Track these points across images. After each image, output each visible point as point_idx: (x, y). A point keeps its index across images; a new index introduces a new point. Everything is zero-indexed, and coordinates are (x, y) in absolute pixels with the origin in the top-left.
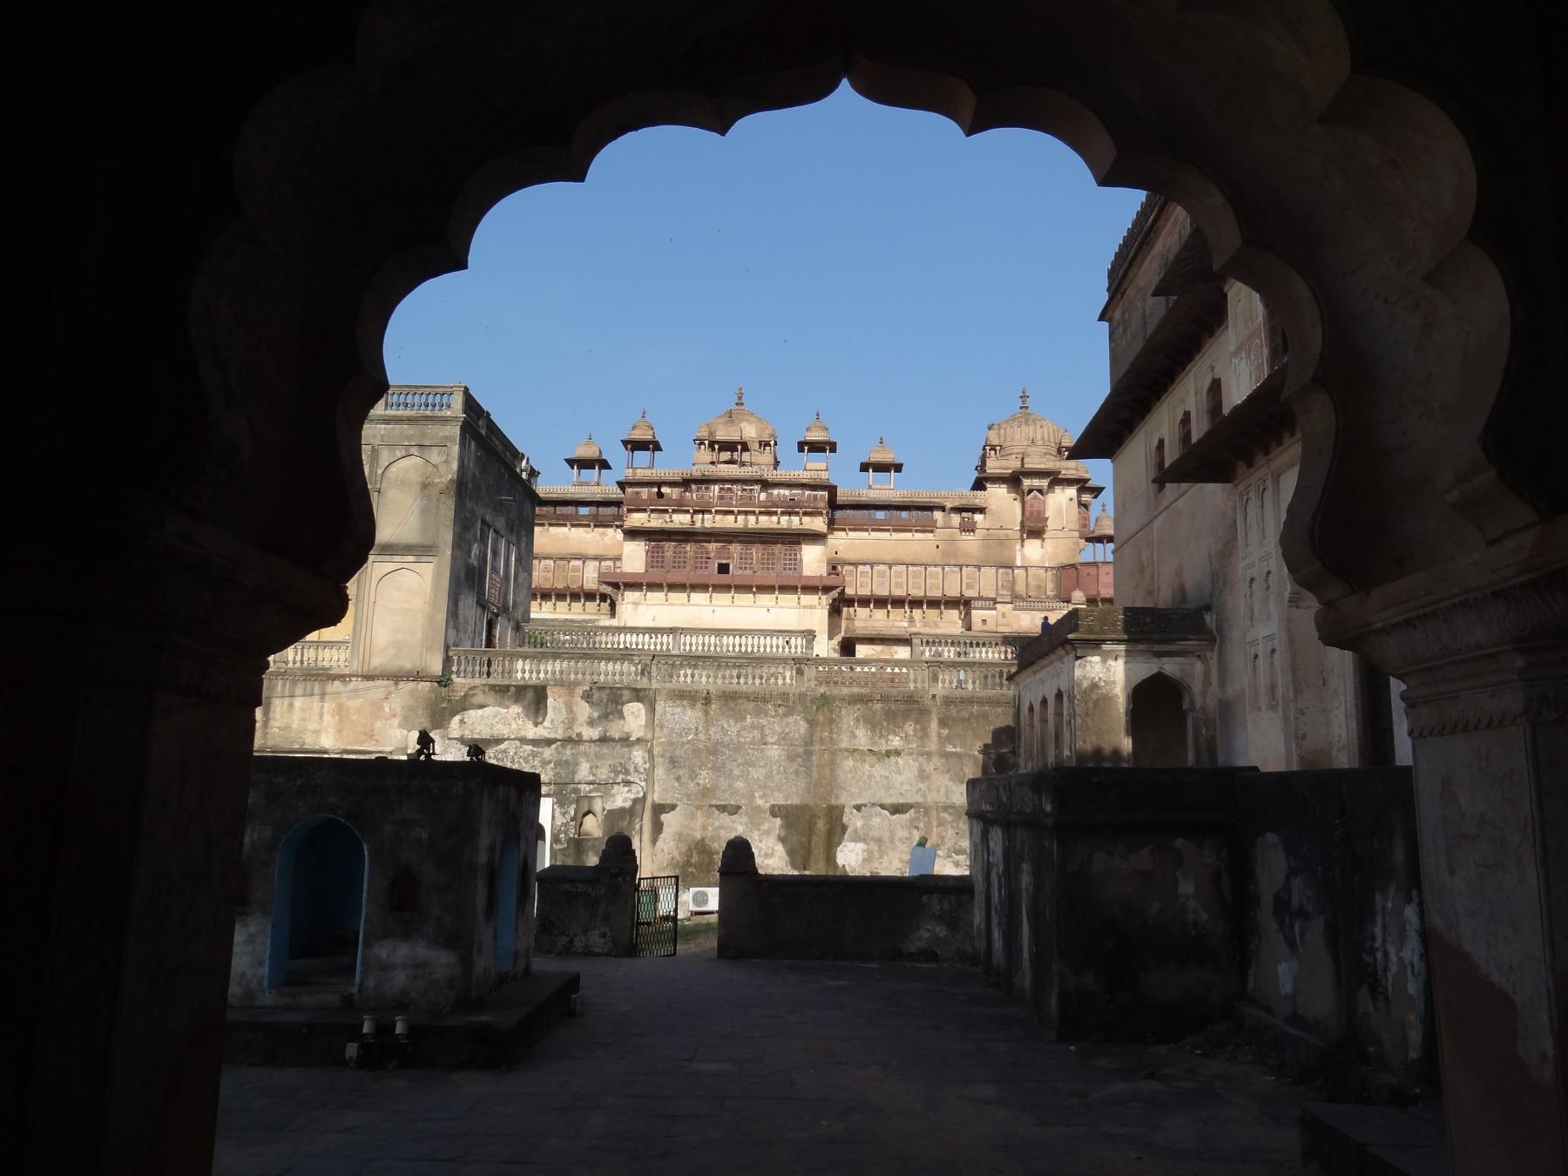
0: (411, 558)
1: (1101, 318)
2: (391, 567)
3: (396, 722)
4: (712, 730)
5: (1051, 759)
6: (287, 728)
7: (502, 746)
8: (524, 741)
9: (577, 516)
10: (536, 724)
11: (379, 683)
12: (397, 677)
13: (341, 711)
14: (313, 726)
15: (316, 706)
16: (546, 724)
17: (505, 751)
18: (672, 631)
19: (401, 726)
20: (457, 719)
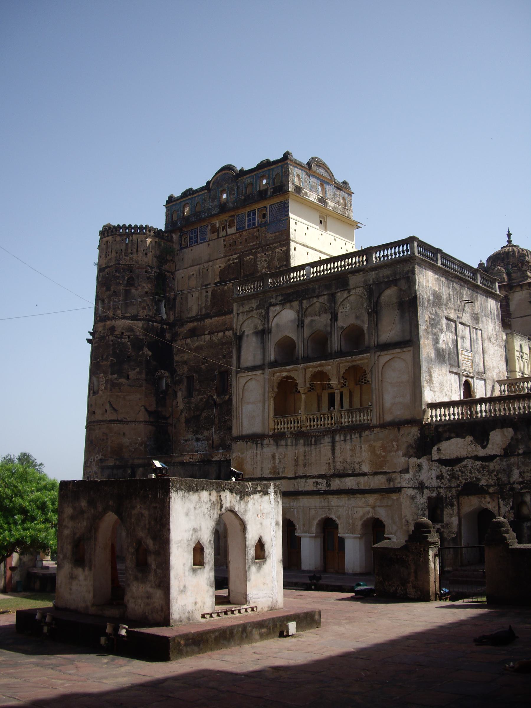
0: (398, 350)
2: (388, 357)
5: (241, 434)
7: (464, 463)
8: (476, 458)
9: (485, 306)
10: (484, 447)
16: (489, 446)
17: (465, 466)
19: (404, 455)
20: (435, 448)
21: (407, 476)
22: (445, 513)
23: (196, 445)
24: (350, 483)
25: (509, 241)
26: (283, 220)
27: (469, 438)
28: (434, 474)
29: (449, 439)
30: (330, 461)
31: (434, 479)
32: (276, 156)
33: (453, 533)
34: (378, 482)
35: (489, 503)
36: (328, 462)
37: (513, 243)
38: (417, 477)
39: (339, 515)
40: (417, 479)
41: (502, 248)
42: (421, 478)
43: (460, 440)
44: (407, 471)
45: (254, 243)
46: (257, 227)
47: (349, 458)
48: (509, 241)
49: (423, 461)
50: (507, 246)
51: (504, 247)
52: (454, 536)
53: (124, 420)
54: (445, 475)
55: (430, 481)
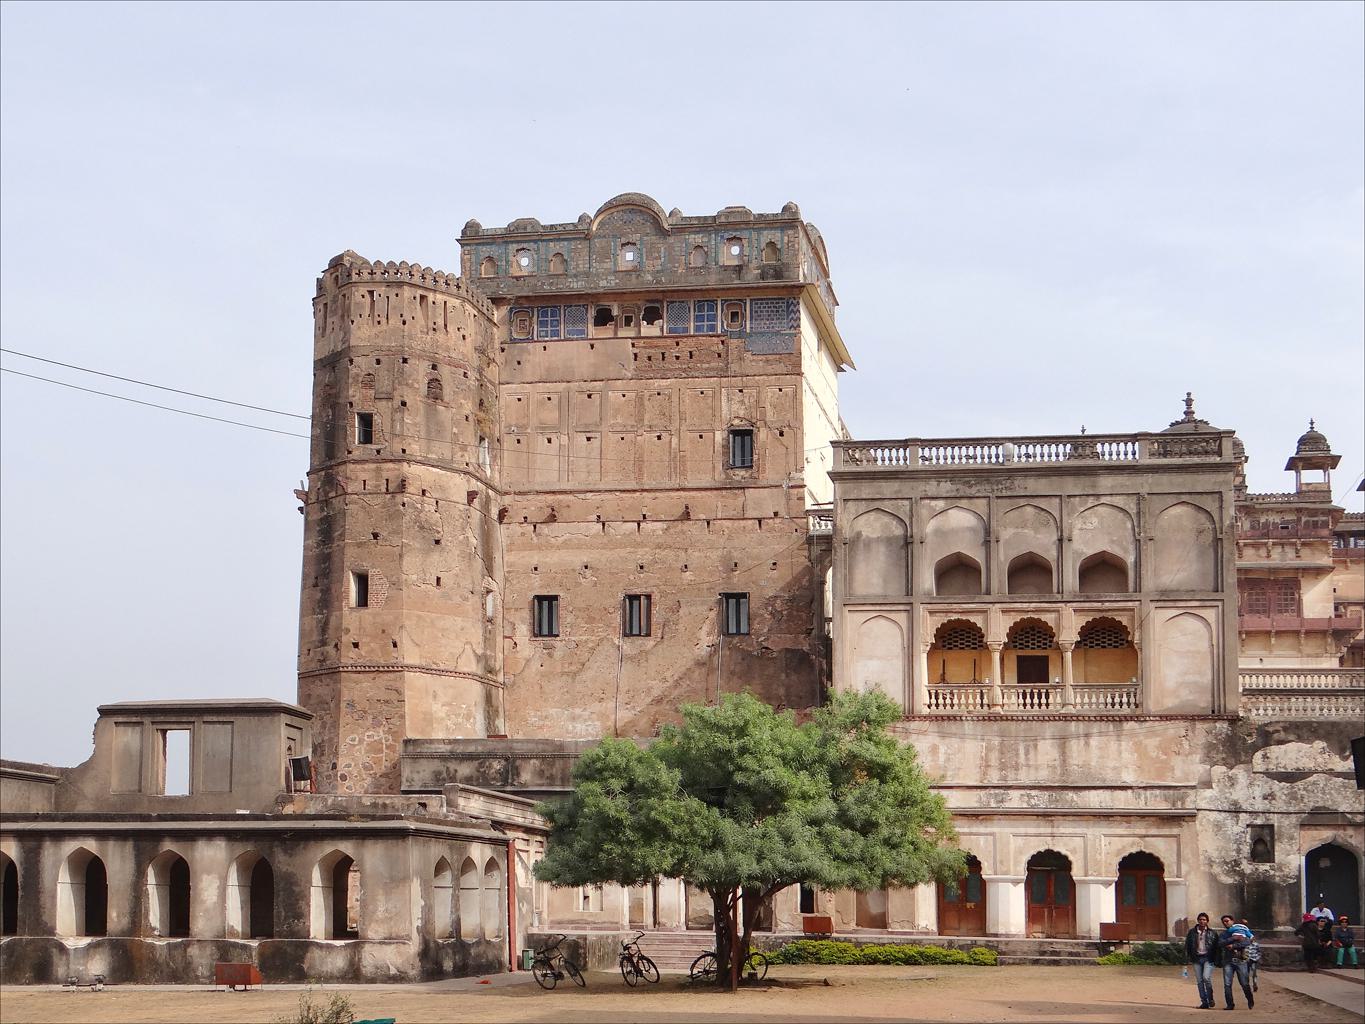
1: (1288, 468)
3: (1197, 757)
4: (454, 566)
6: (1086, 765)
11: (554, 797)
12: (1192, 718)
13: (1139, 748)
14: (1111, 764)
15: (1113, 745)
17: (1314, 783)
18: (905, 444)
19: (1203, 762)
20: (1258, 755)
21: (1208, 793)
22: (1277, 848)
23: (570, 728)
24: (1095, 800)
25: (1189, 413)
26: (786, 335)
27: (1320, 744)
28: (1258, 792)
29: (1281, 742)
30: (1057, 763)
31: (1259, 800)
32: (767, 204)
33: (1291, 878)
34: (1157, 803)
35: (1351, 837)
36: (1051, 764)
37: (1197, 416)
38: (1228, 795)
39: (1075, 848)
40: (1226, 798)
41: (1172, 425)
42: (1235, 797)
43: (1305, 746)
44: (1208, 785)
45: (713, 364)
46: (719, 336)
47: (1095, 760)
48: (1189, 413)
49: (1239, 772)
50: (1183, 422)
51: (1177, 423)
52: (1292, 881)
53: (434, 667)
54: (1278, 794)
55: (1252, 801)
